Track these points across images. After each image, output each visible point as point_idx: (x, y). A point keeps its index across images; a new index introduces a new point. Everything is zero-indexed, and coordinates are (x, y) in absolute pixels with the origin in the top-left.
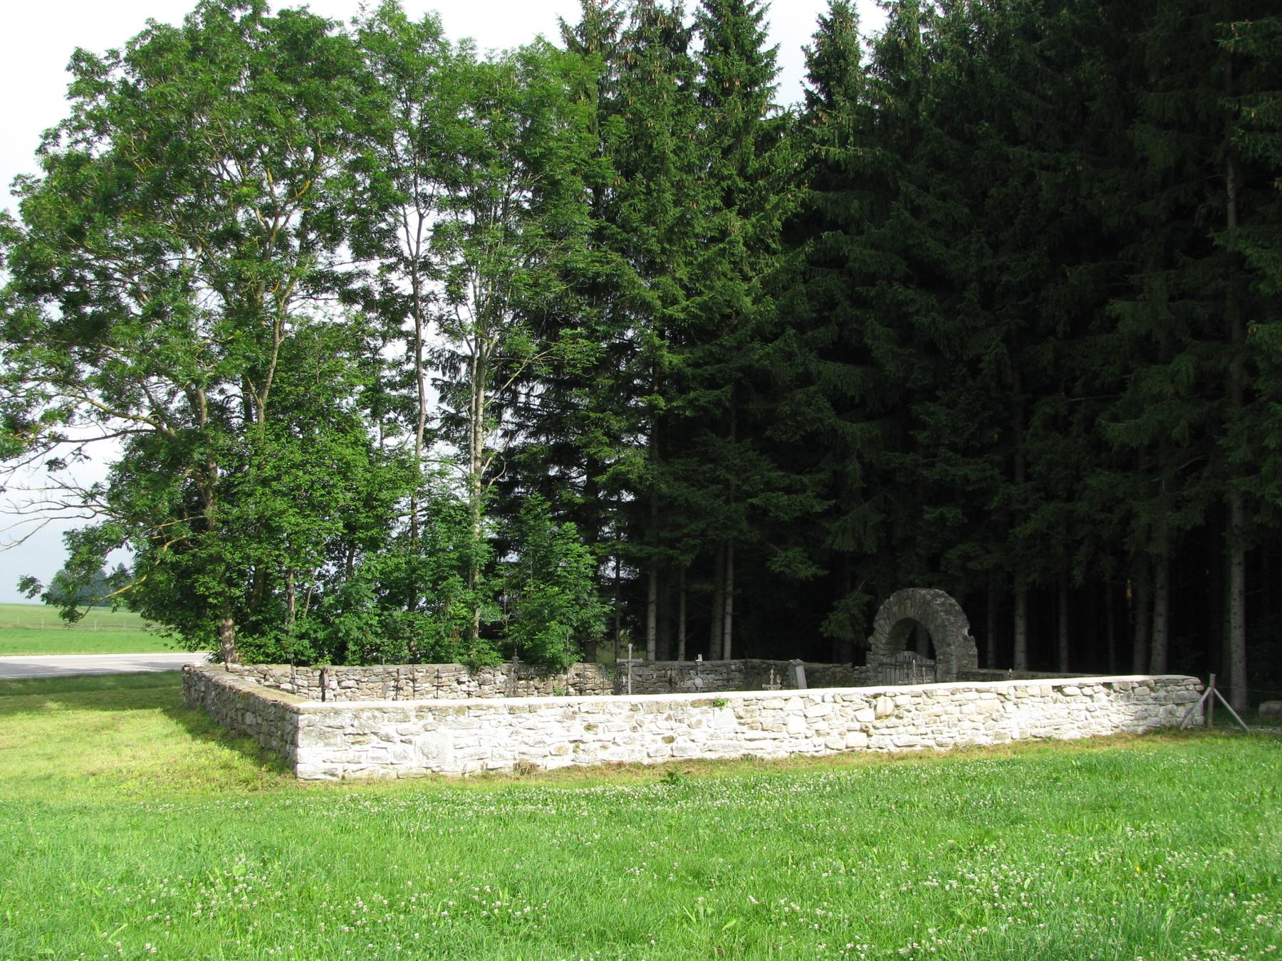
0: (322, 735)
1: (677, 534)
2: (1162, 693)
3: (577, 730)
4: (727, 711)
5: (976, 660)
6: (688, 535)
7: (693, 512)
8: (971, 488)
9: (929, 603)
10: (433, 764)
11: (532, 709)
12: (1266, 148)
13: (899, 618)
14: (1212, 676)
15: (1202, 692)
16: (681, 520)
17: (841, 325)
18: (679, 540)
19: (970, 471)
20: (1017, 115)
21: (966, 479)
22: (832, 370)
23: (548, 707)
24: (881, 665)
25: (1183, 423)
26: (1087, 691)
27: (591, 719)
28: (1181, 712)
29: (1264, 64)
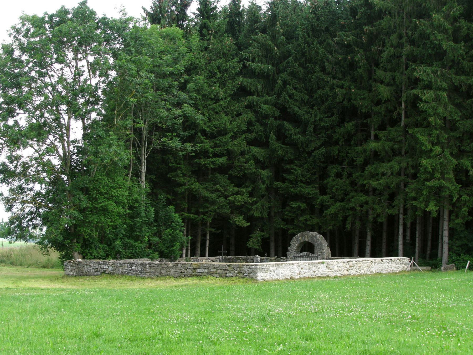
0: (261, 271)
1: (206, 210)
2: (402, 262)
3: (300, 270)
4: (325, 265)
5: (330, 254)
6: (211, 211)
7: (213, 203)
8: (310, 197)
9: (315, 237)
10: (278, 277)
11: (293, 264)
12: (426, 108)
13: (302, 241)
14: (413, 257)
15: (410, 262)
16: (208, 205)
17: (257, 133)
18: (207, 212)
19: (309, 190)
20: (327, 64)
21: (308, 193)
22: (255, 150)
23: (296, 263)
24: (294, 256)
25: (394, 183)
26: (387, 261)
27: (302, 266)
28: (406, 267)
29: (426, 82)
